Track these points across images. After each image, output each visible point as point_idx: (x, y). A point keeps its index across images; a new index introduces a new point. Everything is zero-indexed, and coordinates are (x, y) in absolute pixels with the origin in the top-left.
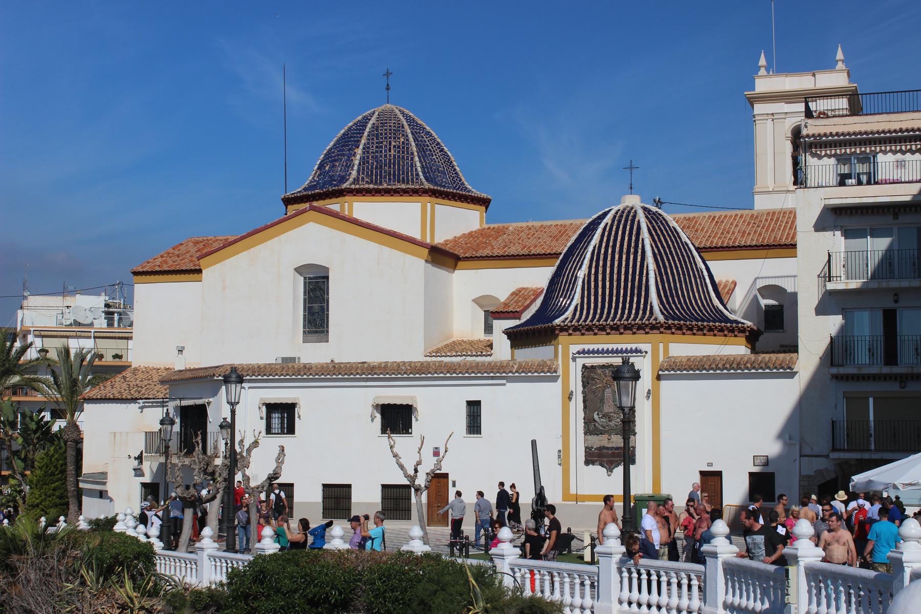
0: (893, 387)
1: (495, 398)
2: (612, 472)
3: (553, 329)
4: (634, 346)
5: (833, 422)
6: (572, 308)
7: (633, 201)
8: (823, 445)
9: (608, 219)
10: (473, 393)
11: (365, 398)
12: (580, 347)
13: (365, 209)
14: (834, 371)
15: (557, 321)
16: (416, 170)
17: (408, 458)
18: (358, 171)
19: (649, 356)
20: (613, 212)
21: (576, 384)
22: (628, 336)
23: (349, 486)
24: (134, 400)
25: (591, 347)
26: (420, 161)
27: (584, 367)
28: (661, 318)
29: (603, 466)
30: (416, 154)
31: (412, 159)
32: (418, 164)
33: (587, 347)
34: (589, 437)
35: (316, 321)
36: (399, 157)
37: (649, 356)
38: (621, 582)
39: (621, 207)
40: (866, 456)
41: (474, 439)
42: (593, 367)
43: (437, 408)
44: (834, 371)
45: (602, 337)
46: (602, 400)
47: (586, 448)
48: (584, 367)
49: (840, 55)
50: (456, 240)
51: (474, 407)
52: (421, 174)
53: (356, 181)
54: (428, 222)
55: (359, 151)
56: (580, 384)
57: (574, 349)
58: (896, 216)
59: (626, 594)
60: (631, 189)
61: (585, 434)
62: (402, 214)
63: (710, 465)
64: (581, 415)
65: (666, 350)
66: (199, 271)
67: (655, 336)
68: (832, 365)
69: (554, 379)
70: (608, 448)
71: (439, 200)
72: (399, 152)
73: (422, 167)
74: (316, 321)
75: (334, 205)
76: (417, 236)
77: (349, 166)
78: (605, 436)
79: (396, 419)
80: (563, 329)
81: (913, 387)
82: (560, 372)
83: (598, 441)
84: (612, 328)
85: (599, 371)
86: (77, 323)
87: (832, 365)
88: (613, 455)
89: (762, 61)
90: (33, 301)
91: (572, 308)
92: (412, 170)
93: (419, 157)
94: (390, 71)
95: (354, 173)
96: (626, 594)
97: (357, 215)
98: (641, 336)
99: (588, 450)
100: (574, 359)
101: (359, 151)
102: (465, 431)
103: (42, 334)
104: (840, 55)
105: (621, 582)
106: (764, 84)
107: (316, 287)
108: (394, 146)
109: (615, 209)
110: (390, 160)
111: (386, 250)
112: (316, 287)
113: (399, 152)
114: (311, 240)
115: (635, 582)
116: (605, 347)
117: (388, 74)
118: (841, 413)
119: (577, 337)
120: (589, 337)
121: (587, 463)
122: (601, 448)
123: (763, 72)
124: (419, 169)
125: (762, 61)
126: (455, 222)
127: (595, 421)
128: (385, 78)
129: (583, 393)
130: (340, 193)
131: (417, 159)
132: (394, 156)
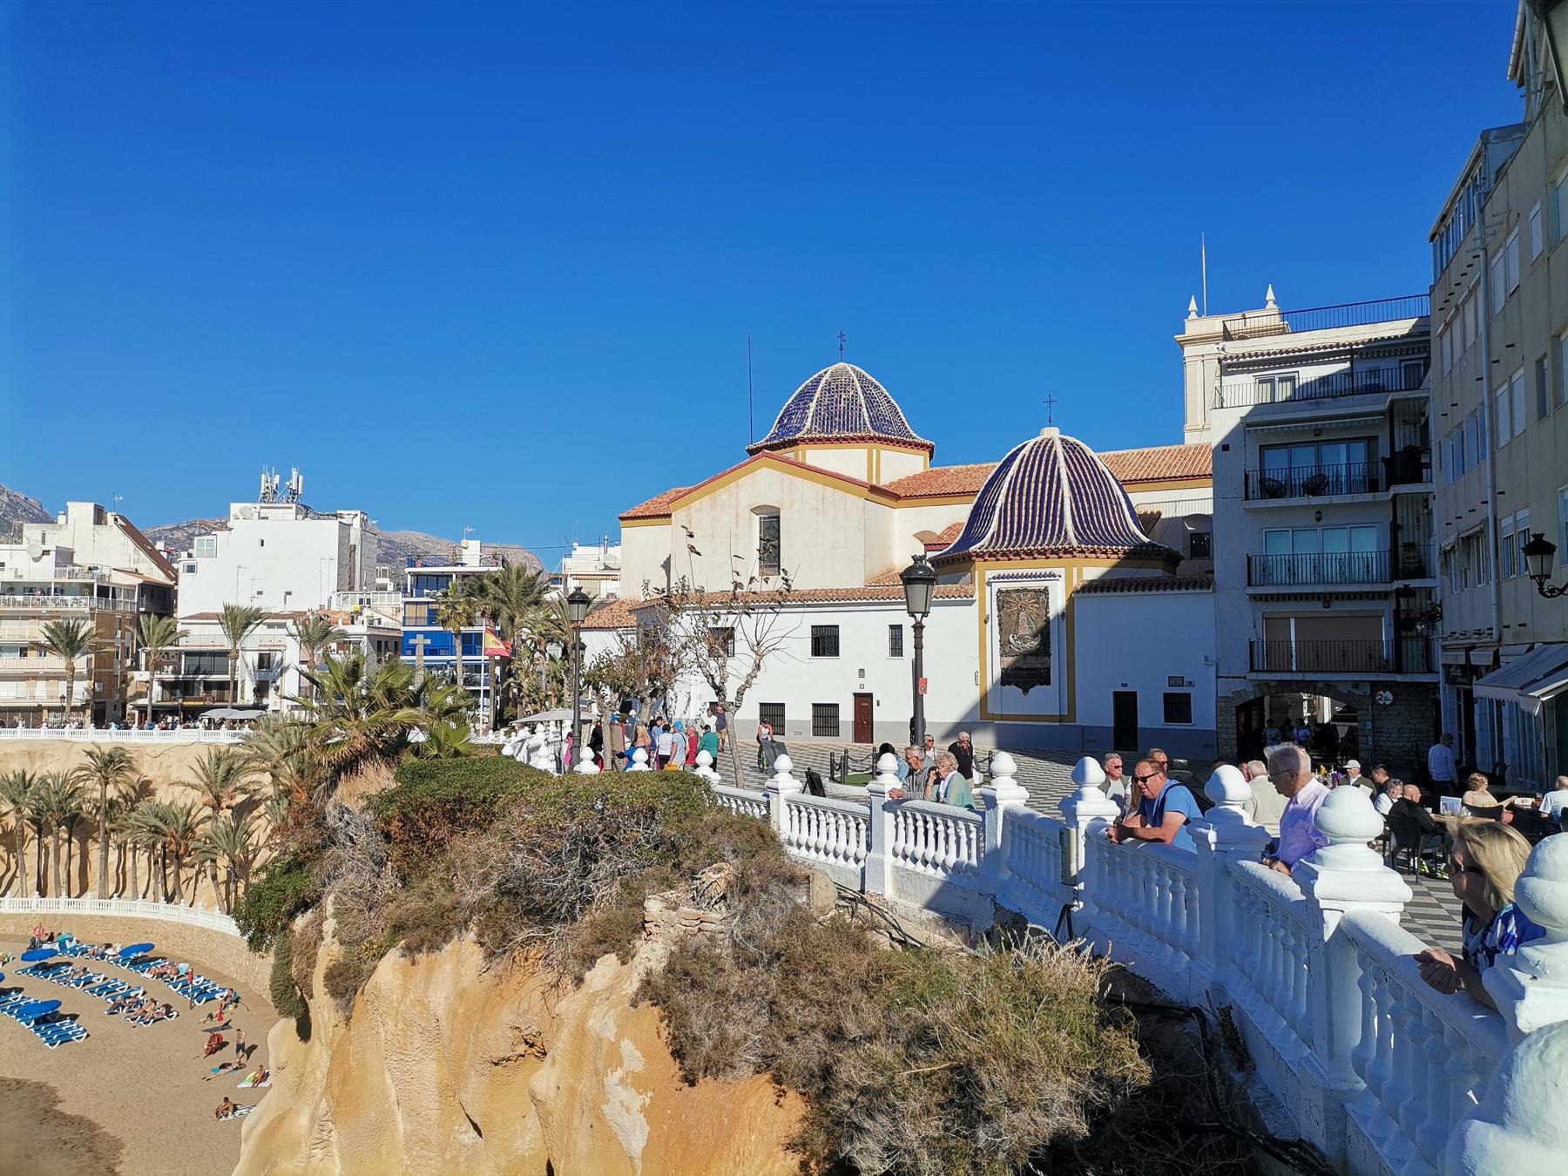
0: (1316, 607)
3: (970, 556)
4: (1048, 571)
5: (1251, 643)
6: (988, 536)
7: (1052, 433)
8: (1240, 664)
9: (1025, 451)
11: (798, 626)
12: (996, 573)
13: (816, 456)
14: (1251, 590)
15: (973, 548)
17: (834, 682)
20: (1028, 448)
21: (992, 610)
22: (1041, 560)
23: (783, 705)
24: (614, 628)
25: (1006, 572)
27: (1000, 591)
28: (1075, 543)
33: (1002, 572)
35: (770, 553)
37: (1062, 580)
38: (897, 826)
39: (1039, 439)
40: (1287, 677)
43: (863, 631)
44: (1251, 590)
45: (1016, 561)
48: (1000, 591)
49: (1270, 295)
50: (900, 482)
53: (809, 431)
54: (873, 465)
55: (813, 405)
56: (995, 607)
57: (989, 574)
59: (901, 844)
60: (1050, 423)
62: (850, 460)
63: (1124, 685)
64: (997, 637)
65: (1080, 574)
66: (669, 516)
67: (1067, 559)
68: (1249, 584)
69: (971, 603)
74: (770, 553)
75: (789, 453)
76: (864, 479)
77: (803, 419)
79: (825, 643)
80: (980, 555)
82: (976, 597)
84: (1004, 554)
86: (607, 568)
87: (1249, 584)
89: (1193, 306)
90: (580, 551)
91: (988, 536)
95: (808, 424)
96: (901, 844)
97: (809, 462)
98: (1053, 559)
100: (989, 584)
101: (813, 405)
103: (576, 577)
104: (1270, 295)
105: (897, 826)
106: (1196, 326)
107: (771, 525)
109: (1033, 441)
111: (830, 490)
112: (771, 525)
114: (765, 483)
115: (921, 831)
116: (1020, 572)
118: (1259, 634)
119: (992, 562)
120: (1004, 562)
123: (1193, 315)
125: (1193, 306)
126: (900, 465)
130: (794, 443)
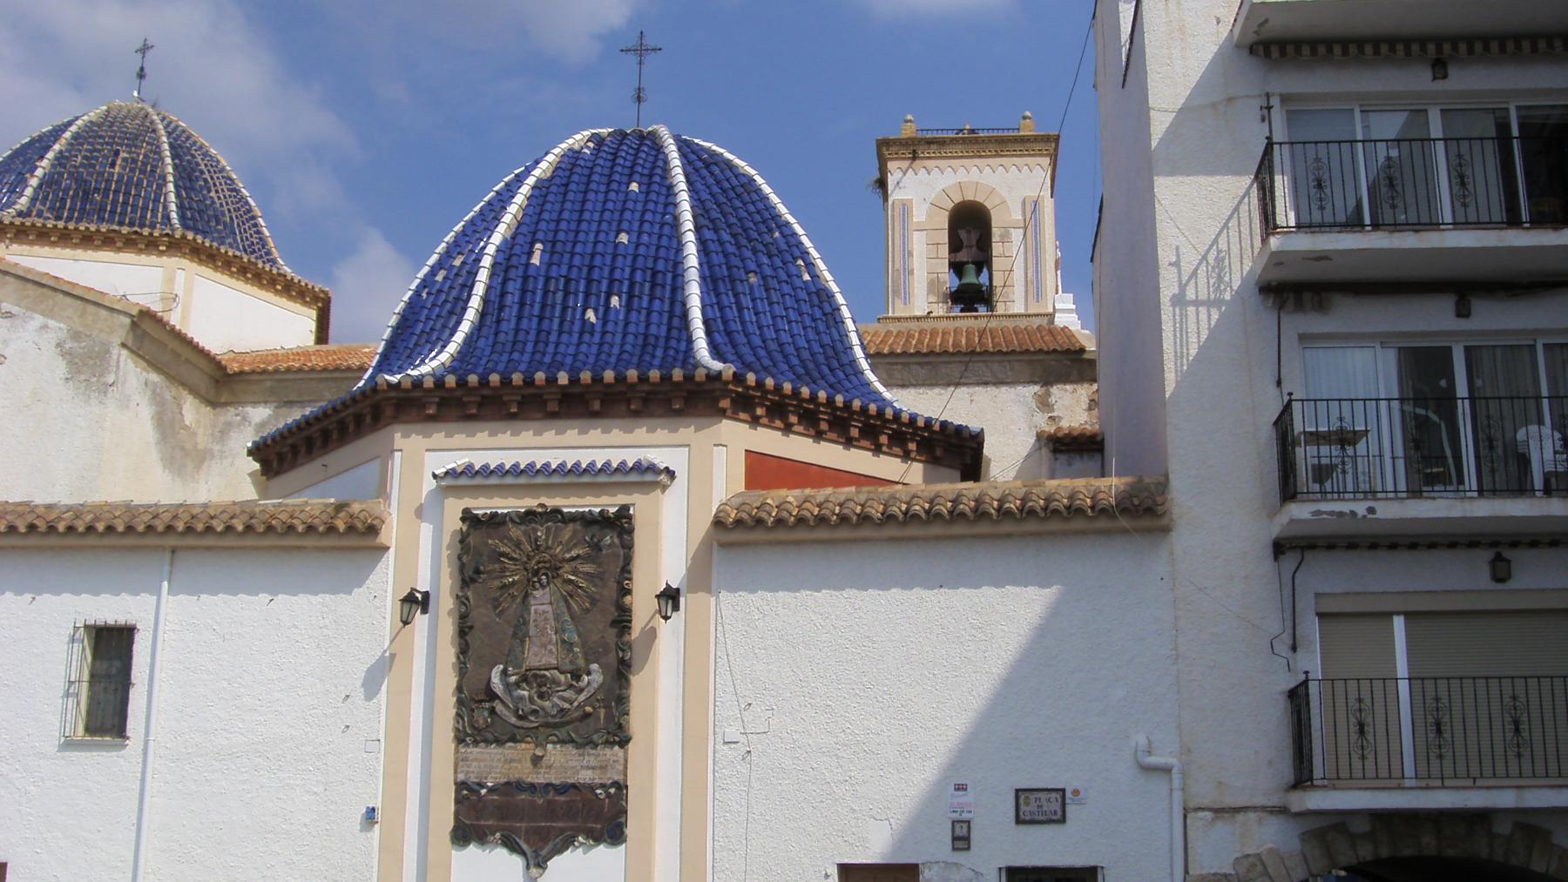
0: (1462, 577)
1: (187, 631)
2: (542, 865)
10: (110, 609)
16: (165, 208)
18: (33, 200)
19: (678, 489)
26: (178, 195)
27: (467, 516)
29: (514, 848)
30: (171, 178)
31: (160, 187)
32: (172, 197)
34: (474, 751)
36: (130, 179)
41: (106, 766)
42: (494, 522)
46: (520, 631)
47: (461, 786)
48: (467, 516)
51: (111, 647)
52: (174, 215)
58: (1440, 67)
61: (460, 739)
70: (532, 788)
71: (206, 271)
72: (132, 170)
73: (181, 207)
78: (525, 749)
81: (1537, 577)
83: (497, 764)
85: (515, 532)
88: (551, 811)
92: (157, 201)
93: (176, 186)
94: (149, 43)
99: (466, 793)
102: (447, 838)
108: (124, 160)
110: (108, 181)
113: (132, 170)
117: (145, 49)
121: (463, 835)
122: (512, 787)
124: (173, 207)
127: (492, 696)
128: (139, 55)
129: (461, 600)
131: (171, 187)
132: (121, 176)
